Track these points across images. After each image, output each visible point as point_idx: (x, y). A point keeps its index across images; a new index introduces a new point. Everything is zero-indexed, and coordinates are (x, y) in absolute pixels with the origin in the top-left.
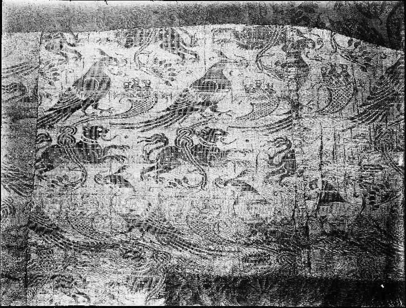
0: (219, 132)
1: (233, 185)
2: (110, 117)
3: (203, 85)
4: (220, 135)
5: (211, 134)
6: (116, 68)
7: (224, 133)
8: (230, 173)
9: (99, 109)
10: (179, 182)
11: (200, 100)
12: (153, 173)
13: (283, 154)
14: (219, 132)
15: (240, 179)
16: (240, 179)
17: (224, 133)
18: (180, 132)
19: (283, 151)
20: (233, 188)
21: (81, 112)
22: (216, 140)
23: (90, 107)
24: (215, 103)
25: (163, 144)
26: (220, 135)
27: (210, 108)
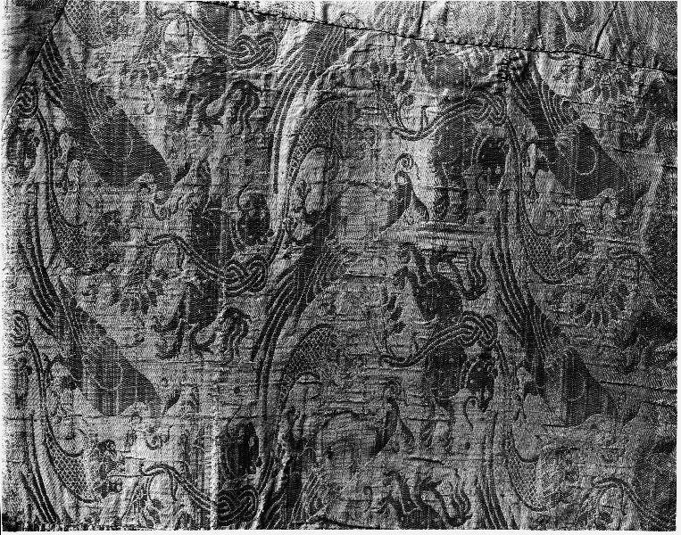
0: (486, 395)
1: (388, 413)
2: (49, 183)
3: (575, 371)
4: (483, 398)
5: (483, 381)
6: (613, 214)
7: (484, 405)
8: (412, 411)
9: (536, 172)
10: (395, 317)
11: (548, 365)
12: (412, 265)
13: (438, 507)
14: (486, 395)
15: (398, 427)
16: (398, 427)
17: (484, 405)
18: (488, 322)
19: (460, 282)
20: (383, 413)
21: (533, 135)
22: (472, 388)
23: (67, 373)
24: (542, 393)
25: (468, 288)
26: (483, 398)
27: (532, 382)
